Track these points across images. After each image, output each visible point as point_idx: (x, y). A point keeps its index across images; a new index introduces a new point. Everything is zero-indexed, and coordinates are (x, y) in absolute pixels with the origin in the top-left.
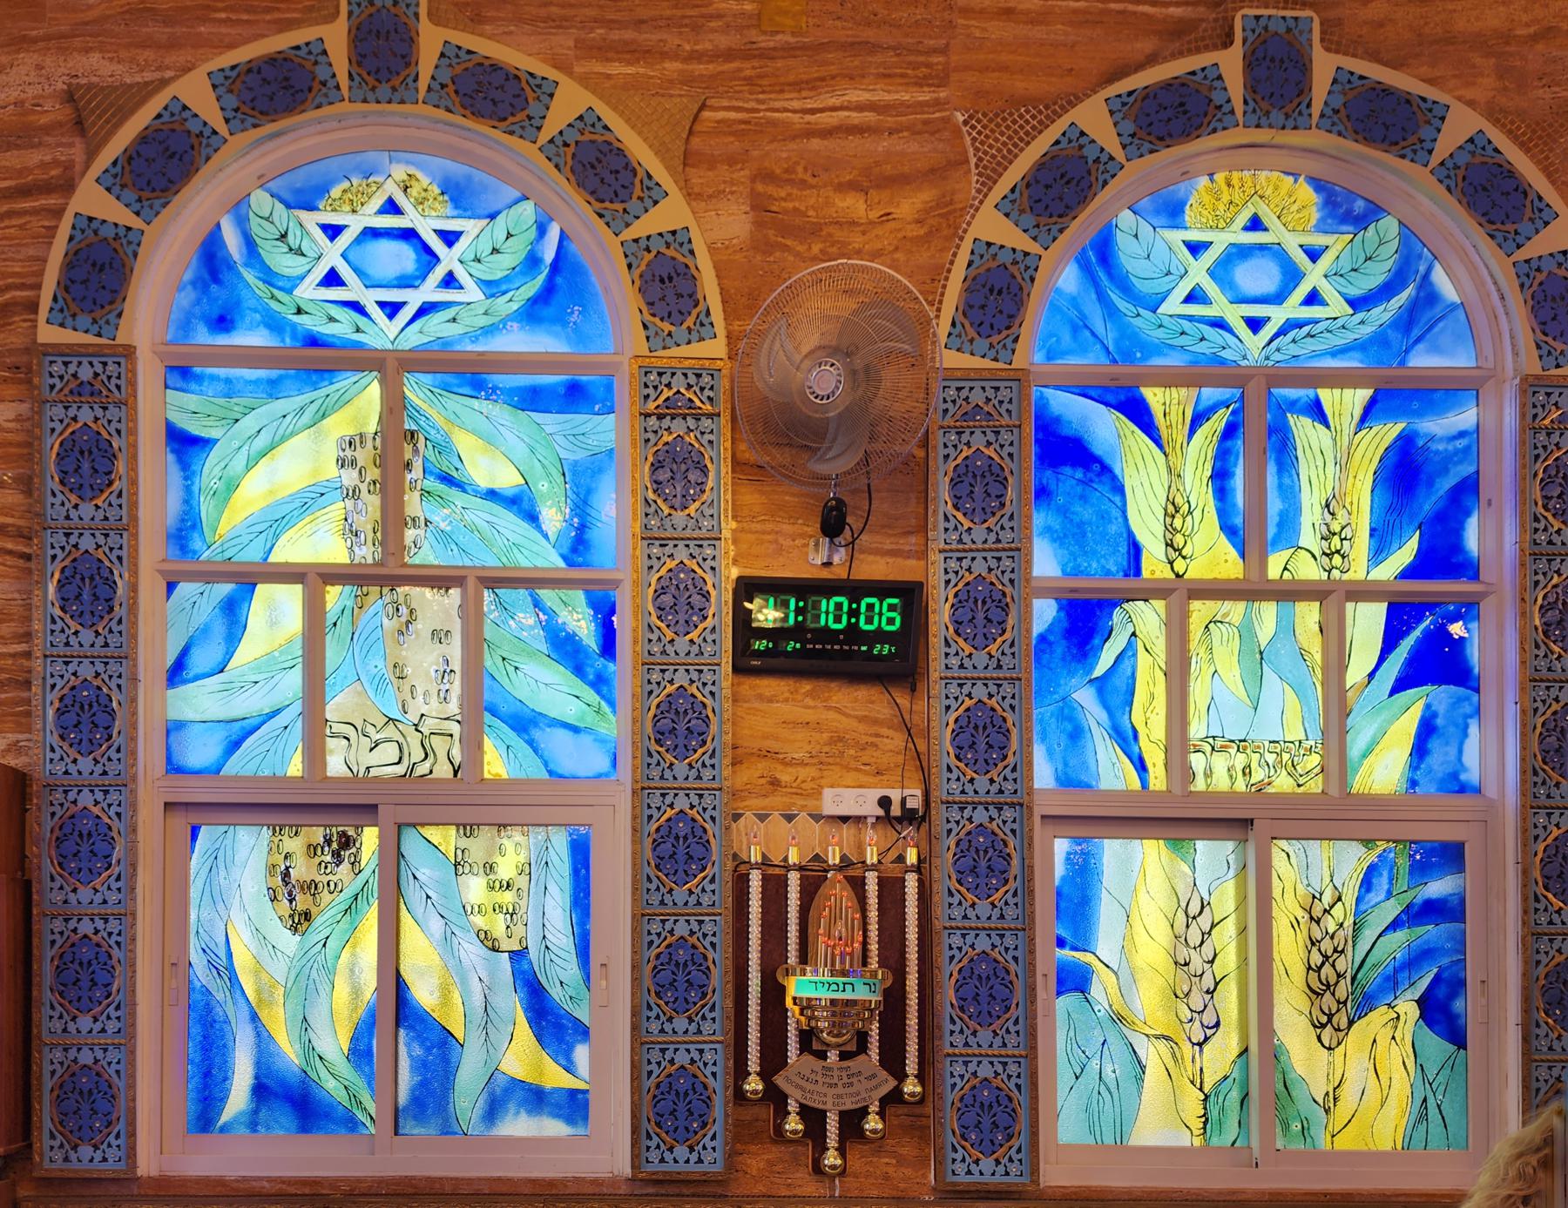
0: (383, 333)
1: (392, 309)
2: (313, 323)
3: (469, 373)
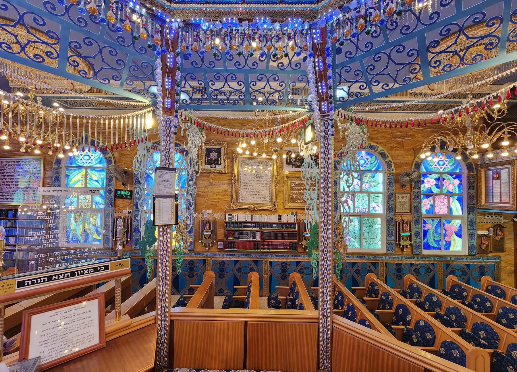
0: (86, 165)
1: (86, 162)
2: (80, 164)
3: (93, 168)
